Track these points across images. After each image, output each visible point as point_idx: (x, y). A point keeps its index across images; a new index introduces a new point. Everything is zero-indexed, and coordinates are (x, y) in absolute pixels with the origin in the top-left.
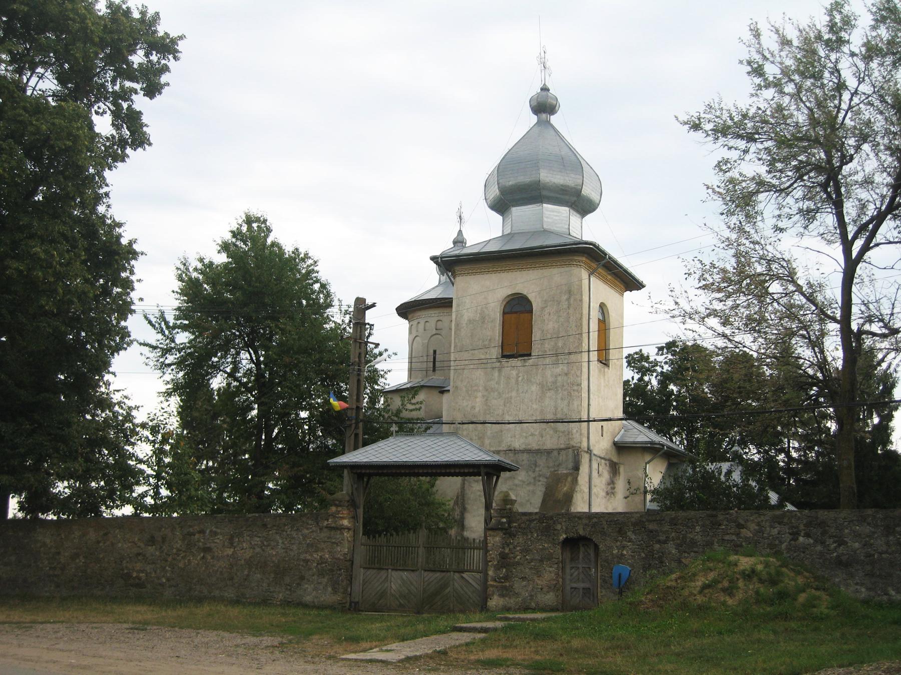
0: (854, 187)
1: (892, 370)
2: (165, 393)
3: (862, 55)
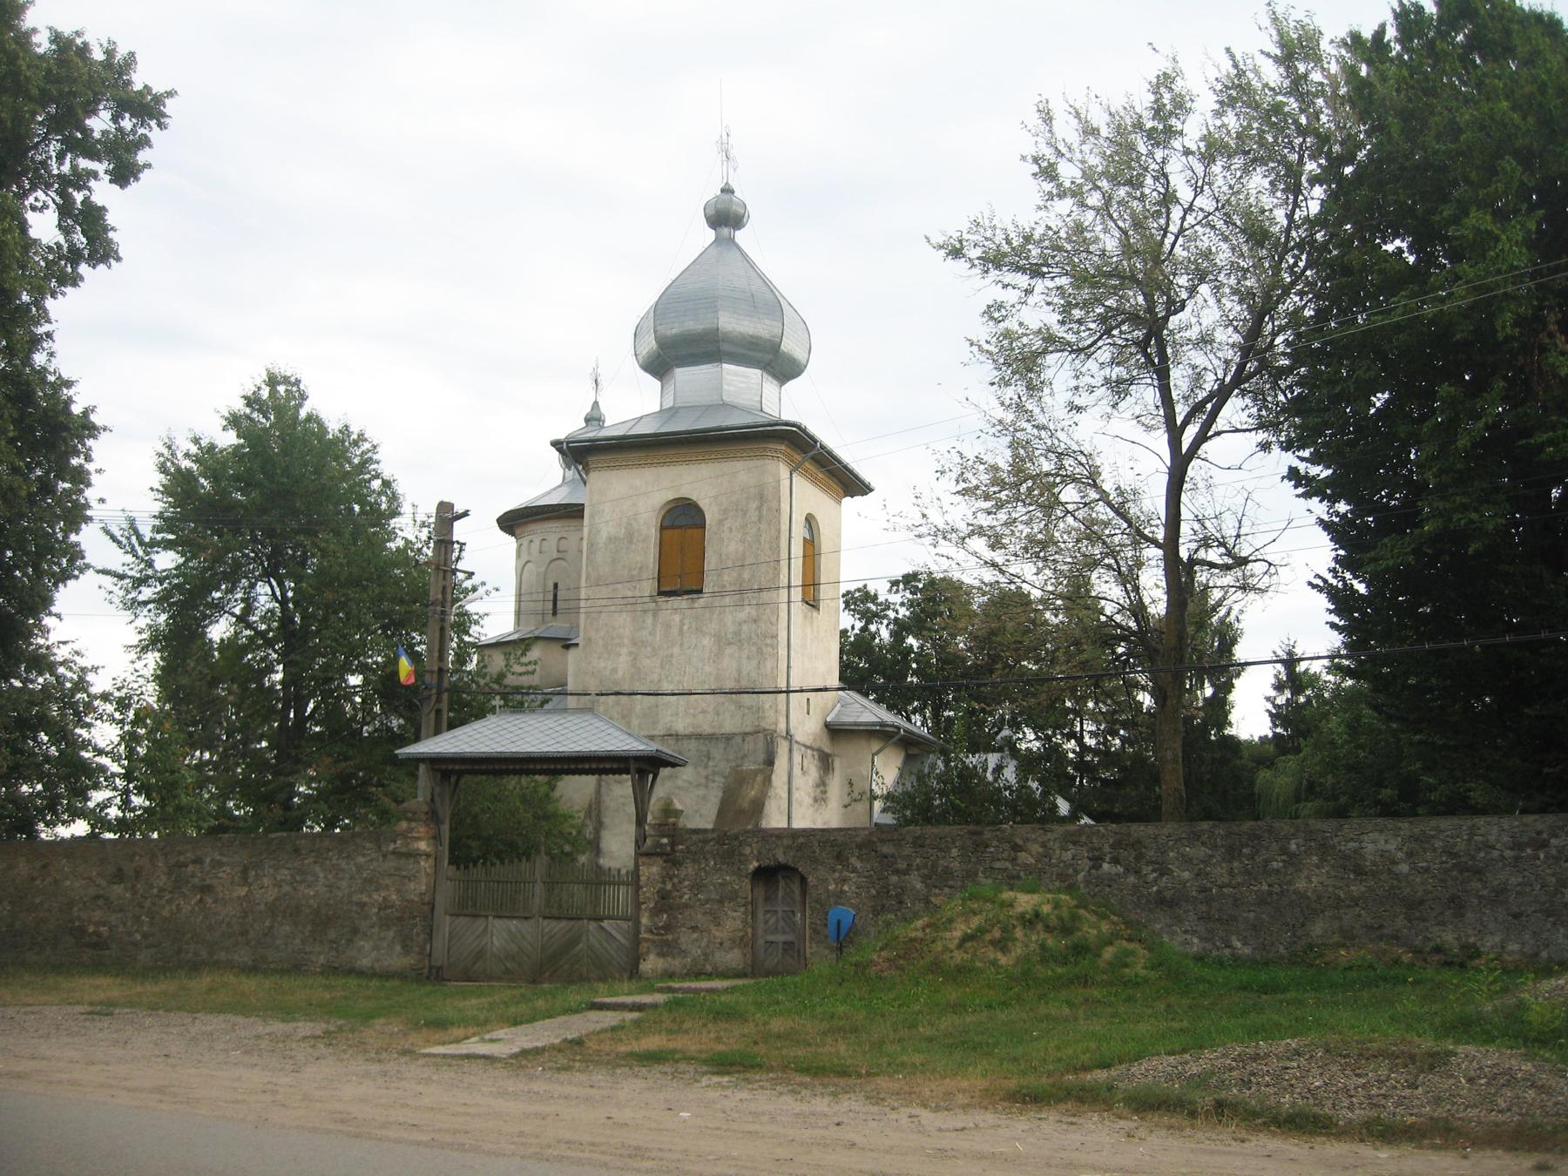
0: (1185, 348)
1: (1232, 618)
2: (136, 647)
3: (1201, 153)
